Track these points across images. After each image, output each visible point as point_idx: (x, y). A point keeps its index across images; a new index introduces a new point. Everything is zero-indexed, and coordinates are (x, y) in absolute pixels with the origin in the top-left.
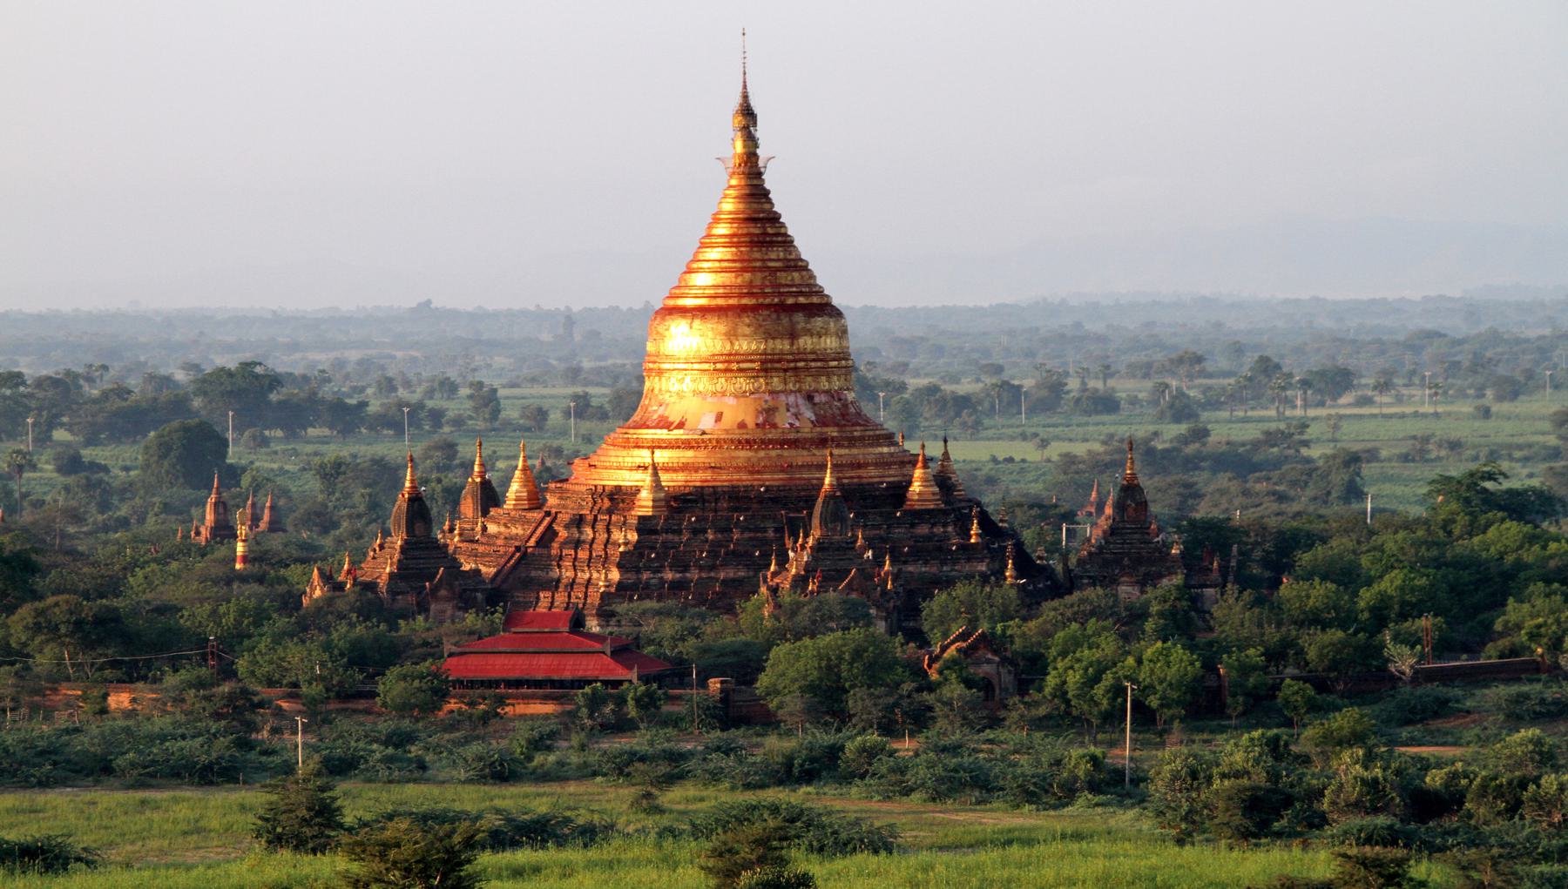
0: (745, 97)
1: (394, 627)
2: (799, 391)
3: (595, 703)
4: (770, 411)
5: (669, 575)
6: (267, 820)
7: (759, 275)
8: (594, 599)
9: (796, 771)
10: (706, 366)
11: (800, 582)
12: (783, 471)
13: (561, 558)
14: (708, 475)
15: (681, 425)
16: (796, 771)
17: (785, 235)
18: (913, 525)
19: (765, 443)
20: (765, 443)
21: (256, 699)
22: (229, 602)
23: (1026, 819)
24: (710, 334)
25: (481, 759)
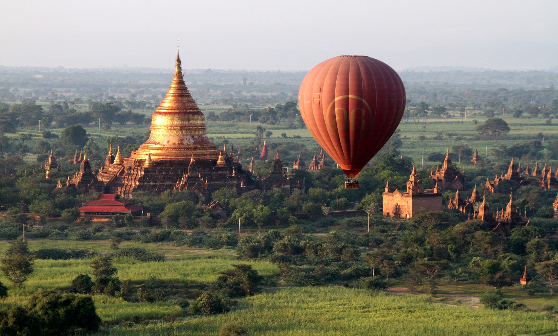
0: (178, 57)
1: (75, 197)
2: (190, 135)
3: (117, 219)
4: (182, 140)
5: (152, 184)
6: (9, 251)
7: (180, 104)
8: (131, 189)
9: (159, 238)
10: (165, 128)
11: (183, 186)
12: (184, 156)
13: (125, 178)
14: (164, 157)
15: (158, 143)
16: (159, 238)
17: (189, 93)
18: (218, 171)
19: (180, 149)
20: (180, 149)
21: (27, 217)
22: (32, 189)
23: (210, 252)
24: (167, 119)
25: (80, 234)
